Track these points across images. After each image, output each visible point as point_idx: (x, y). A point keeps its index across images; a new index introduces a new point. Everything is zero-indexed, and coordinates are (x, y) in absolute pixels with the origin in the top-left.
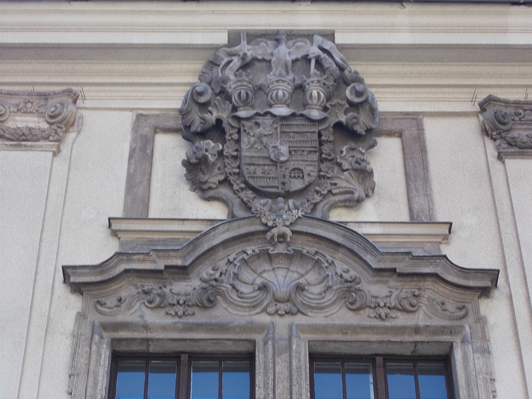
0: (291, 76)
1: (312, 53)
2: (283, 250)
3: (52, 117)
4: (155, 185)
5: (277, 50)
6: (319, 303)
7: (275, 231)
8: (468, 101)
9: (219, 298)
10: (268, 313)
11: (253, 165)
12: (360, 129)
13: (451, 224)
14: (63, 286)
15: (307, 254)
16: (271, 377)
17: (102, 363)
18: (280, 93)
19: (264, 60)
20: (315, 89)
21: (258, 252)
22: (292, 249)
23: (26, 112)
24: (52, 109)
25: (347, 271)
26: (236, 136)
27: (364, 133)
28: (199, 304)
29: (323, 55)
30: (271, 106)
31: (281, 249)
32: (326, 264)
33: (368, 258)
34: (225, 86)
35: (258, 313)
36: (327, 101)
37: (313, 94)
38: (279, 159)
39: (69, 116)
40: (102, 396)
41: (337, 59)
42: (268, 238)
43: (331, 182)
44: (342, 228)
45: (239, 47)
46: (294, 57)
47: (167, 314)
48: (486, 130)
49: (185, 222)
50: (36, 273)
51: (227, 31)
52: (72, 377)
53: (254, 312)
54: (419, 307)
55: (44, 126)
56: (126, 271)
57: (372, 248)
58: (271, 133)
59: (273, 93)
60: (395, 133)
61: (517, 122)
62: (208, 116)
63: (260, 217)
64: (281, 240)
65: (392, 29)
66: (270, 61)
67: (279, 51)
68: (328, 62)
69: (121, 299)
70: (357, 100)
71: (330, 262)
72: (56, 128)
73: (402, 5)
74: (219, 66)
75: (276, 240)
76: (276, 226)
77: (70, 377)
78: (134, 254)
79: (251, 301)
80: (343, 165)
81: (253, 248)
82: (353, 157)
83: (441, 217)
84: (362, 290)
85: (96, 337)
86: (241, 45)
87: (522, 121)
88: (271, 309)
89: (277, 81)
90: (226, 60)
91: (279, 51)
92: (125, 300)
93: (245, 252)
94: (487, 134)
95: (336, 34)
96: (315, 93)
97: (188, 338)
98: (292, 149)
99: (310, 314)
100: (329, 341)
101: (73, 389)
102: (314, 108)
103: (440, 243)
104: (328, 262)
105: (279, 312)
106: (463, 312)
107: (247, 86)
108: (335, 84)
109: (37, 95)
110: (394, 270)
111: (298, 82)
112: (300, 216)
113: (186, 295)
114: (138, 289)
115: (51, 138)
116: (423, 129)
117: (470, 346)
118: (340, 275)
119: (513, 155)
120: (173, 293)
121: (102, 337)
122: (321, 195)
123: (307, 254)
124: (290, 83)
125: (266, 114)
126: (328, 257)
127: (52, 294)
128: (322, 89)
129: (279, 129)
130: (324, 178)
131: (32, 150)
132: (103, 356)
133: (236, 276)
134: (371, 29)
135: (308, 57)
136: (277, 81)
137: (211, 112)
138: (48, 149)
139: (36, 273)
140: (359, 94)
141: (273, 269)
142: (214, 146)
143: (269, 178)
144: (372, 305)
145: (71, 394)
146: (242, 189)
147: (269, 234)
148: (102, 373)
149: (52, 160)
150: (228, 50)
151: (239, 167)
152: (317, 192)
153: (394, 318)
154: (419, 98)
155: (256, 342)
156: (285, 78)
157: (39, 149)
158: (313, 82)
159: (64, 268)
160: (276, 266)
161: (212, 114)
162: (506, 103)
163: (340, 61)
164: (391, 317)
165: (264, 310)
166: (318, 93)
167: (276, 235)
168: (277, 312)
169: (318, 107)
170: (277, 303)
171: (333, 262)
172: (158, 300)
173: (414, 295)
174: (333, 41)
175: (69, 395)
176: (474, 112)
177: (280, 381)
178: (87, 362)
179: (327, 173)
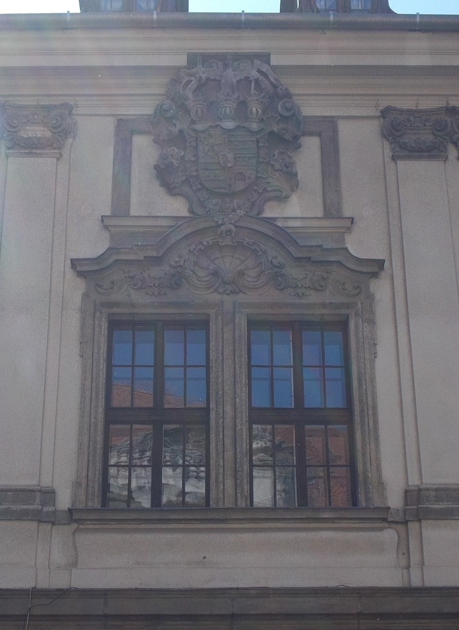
0: (236, 96)
1: (253, 77)
2: (230, 243)
3: (54, 128)
4: (134, 181)
5: (225, 73)
6: (255, 285)
7: (223, 228)
8: (374, 106)
9: (183, 280)
10: (219, 293)
11: (207, 169)
12: (287, 137)
13: (353, 219)
14: (71, 270)
15: (247, 245)
16: (221, 344)
17: (103, 333)
18: (228, 110)
19: (215, 80)
20: (254, 106)
21: (211, 243)
22: (237, 242)
23: (34, 123)
24: (54, 122)
25: (276, 258)
26: (194, 144)
27: (292, 140)
28: (169, 286)
29: (261, 78)
30: (221, 119)
31: (228, 241)
32: (261, 253)
33: (291, 249)
34: (186, 103)
35: (211, 293)
36: (264, 115)
37: (253, 111)
38: (227, 166)
39: (67, 128)
40: (104, 357)
41: (272, 79)
42: (219, 233)
43: (266, 181)
44: (272, 224)
45: (195, 69)
46: (238, 78)
47: (147, 293)
48: (384, 135)
49: (158, 219)
50: (52, 262)
51: (186, 53)
52: (82, 344)
53: (208, 292)
54: (326, 286)
55: (48, 134)
56: (116, 260)
57: (295, 243)
58: (220, 142)
59: (221, 110)
60: (316, 134)
61: (409, 128)
62: (173, 129)
63: (212, 216)
64: (228, 233)
65: (315, 52)
66: (220, 81)
67: (227, 74)
68: (265, 84)
69: (113, 283)
70: (286, 114)
71: (264, 251)
72: (57, 137)
73: (323, 31)
74: (181, 83)
75: (224, 235)
76: (224, 224)
77: (81, 344)
78: (122, 249)
79: (206, 283)
80: (275, 166)
81: (208, 239)
82: (284, 159)
83: (347, 213)
84: (286, 275)
85: (98, 314)
86: (197, 68)
87: (412, 127)
88: (221, 290)
89: (226, 100)
90: (186, 79)
91: (227, 74)
92: (116, 283)
93: (202, 243)
94: (385, 137)
95: (271, 55)
96: (254, 110)
97: (162, 312)
98: (236, 156)
99: (248, 293)
100: (261, 314)
101: (84, 354)
102: (253, 122)
103: (344, 232)
104: (262, 250)
105: (227, 292)
106: (357, 291)
107: (203, 105)
108: (270, 101)
109: (42, 108)
110: (309, 258)
111: (241, 99)
112: (242, 215)
113: (160, 278)
114: (125, 274)
115: (54, 145)
116: (337, 131)
117: (361, 319)
118: (270, 261)
119: (403, 158)
120: (150, 277)
121: (101, 313)
122: (258, 193)
123: (247, 245)
124: (235, 101)
125: (217, 126)
126: (263, 246)
127: (64, 278)
128: (260, 106)
129: (227, 139)
130: (261, 178)
131: (41, 157)
132: (103, 327)
133: (196, 263)
134: (298, 52)
135: (249, 79)
136: (226, 100)
137: (175, 125)
138: (53, 156)
139: (52, 262)
140: (288, 110)
141: (222, 257)
142: (178, 152)
143: (220, 180)
144: (293, 286)
145: (82, 356)
146: (200, 190)
147: (219, 230)
148: (103, 340)
149: (57, 163)
150: (188, 71)
151: (197, 171)
152: (255, 191)
153: (308, 296)
154: (335, 104)
155: (210, 315)
156: (231, 97)
157: (46, 156)
158: (253, 100)
159: (72, 260)
160: (225, 255)
161: (176, 127)
162: (402, 111)
163: (274, 81)
164: (306, 295)
165: (216, 290)
166: (257, 109)
167: (224, 231)
168: (224, 292)
169: (257, 121)
170: (225, 285)
171: (265, 251)
172: (140, 283)
173: (323, 278)
174: (269, 64)
175: (81, 358)
176: (377, 116)
177: (226, 346)
178: (92, 332)
179: (263, 174)
